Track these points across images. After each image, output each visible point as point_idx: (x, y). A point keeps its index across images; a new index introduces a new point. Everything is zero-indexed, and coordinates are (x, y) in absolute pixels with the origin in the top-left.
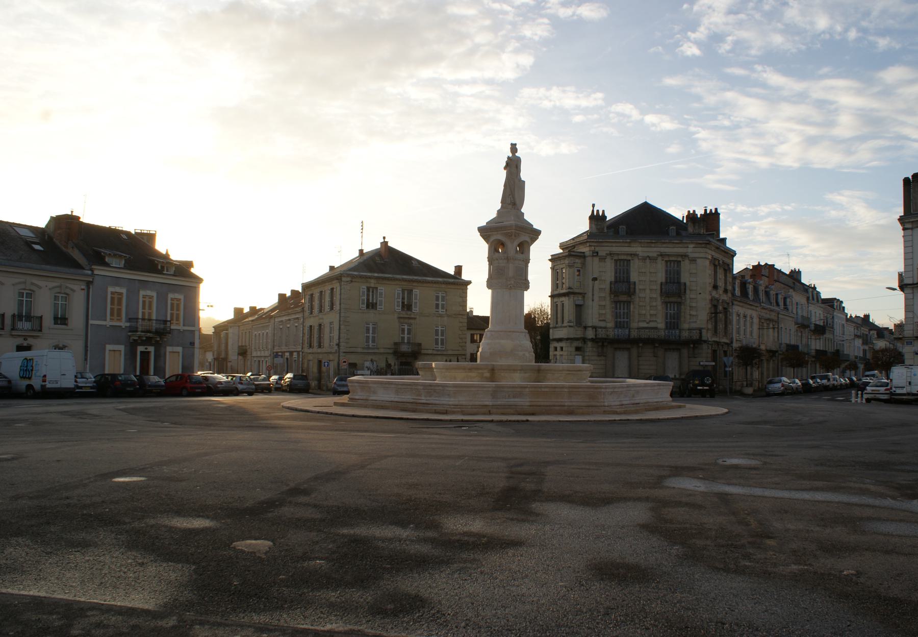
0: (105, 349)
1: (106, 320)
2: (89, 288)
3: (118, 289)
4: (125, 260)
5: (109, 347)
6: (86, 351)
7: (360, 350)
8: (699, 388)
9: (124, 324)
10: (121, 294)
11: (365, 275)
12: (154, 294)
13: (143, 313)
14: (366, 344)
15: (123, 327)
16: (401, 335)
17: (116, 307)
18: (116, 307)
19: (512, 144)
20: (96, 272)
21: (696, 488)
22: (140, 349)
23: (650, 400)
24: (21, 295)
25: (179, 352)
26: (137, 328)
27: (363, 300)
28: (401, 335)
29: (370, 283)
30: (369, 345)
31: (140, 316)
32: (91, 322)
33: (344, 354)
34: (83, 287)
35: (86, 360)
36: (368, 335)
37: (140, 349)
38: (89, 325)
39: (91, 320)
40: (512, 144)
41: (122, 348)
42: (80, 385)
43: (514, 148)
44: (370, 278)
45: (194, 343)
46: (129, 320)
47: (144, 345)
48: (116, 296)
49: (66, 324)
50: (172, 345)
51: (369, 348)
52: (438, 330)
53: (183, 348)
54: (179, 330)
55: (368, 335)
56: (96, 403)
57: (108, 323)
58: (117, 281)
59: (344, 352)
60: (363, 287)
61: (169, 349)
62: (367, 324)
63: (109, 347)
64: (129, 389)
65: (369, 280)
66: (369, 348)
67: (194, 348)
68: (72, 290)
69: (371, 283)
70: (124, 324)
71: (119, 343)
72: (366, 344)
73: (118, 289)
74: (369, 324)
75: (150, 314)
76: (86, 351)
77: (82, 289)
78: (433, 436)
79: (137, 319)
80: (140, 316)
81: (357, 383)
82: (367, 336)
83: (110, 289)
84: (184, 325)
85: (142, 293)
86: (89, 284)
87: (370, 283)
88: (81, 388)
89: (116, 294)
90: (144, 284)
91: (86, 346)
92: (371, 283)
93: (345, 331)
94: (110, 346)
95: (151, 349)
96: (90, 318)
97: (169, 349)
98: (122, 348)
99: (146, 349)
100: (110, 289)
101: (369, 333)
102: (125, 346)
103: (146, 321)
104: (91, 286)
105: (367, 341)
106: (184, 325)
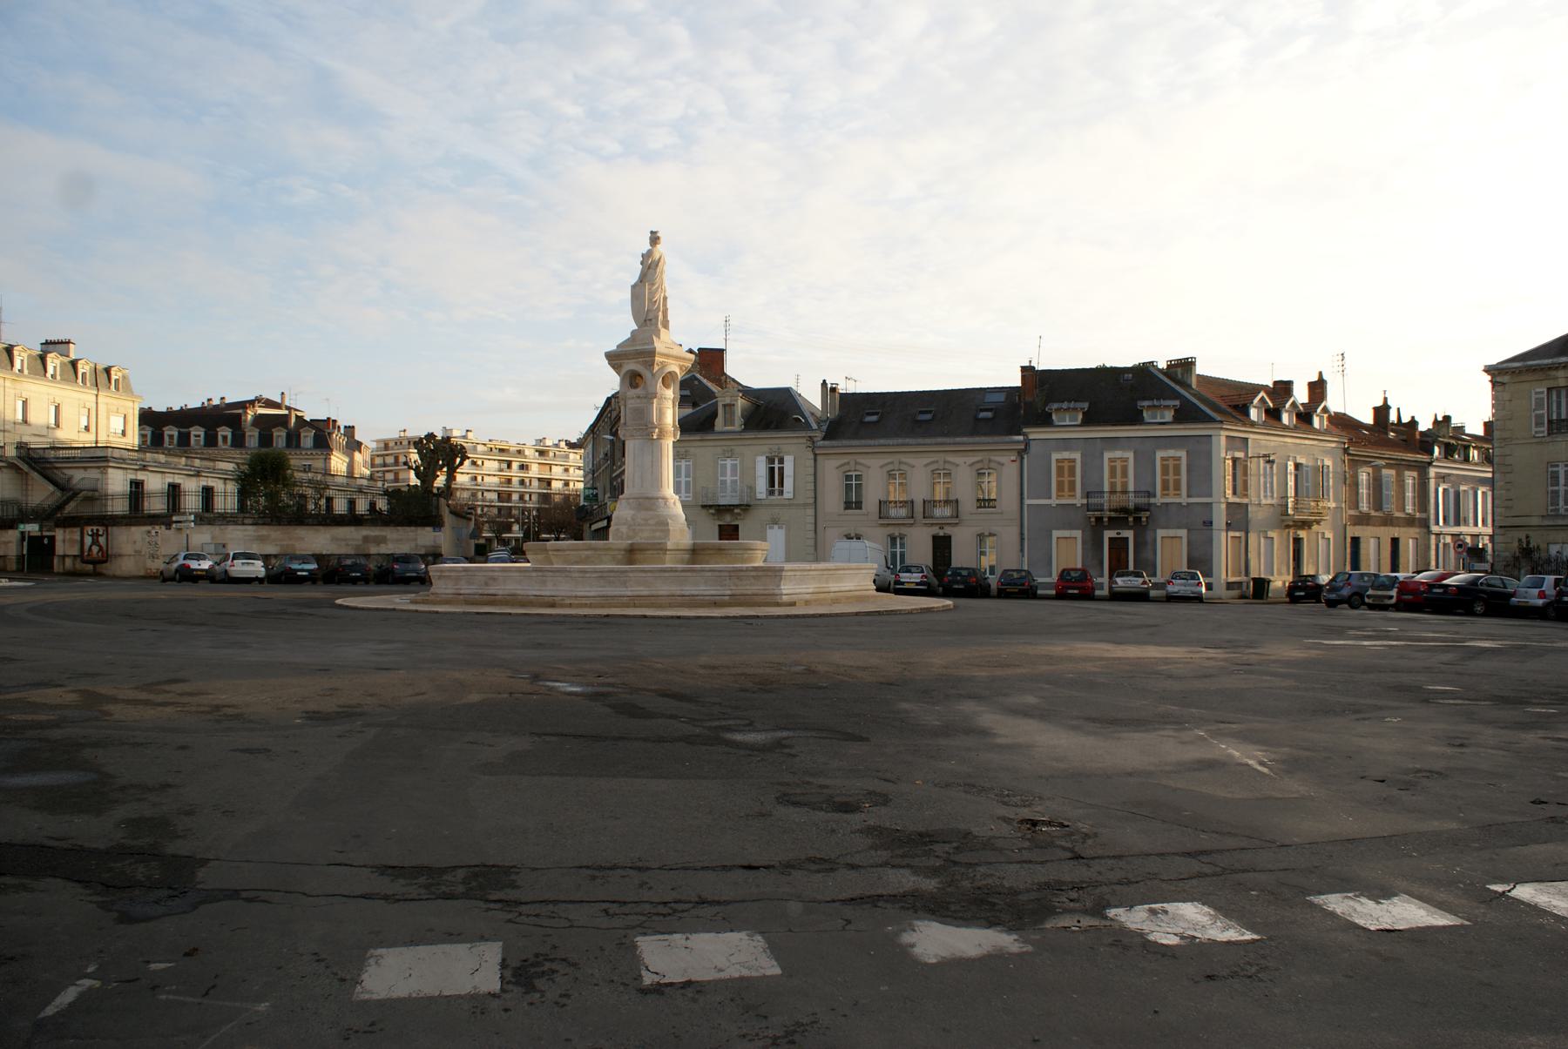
0: (1051, 535)
1: (1050, 498)
2: (1022, 458)
3: (1066, 455)
4: (1083, 413)
5: (1056, 534)
6: (1022, 539)
7: (1535, 521)
8: (1302, 594)
9: (1079, 500)
10: (1074, 461)
11: (1539, 365)
12: (1130, 455)
13: (1112, 485)
14: (1550, 508)
15: (1185, 504)
16: (1550, 488)
17: (1171, 477)
18: (1066, 479)
19: (652, 232)
20: (1031, 437)
21: (420, 697)
22: (1109, 534)
23: (519, 592)
24: (848, 478)
25: (1076, 538)
26: (1102, 505)
27: (1539, 417)
28: (1550, 488)
29: (1556, 378)
30: (1558, 510)
31: (1106, 488)
32: (1027, 502)
33: (1502, 531)
34: (1013, 458)
35: (1022, 550)
36: (1556, 488)
37: (1109, 534)
38: (1026, 506)
39: (1028, 498)
40: (652, 232)
41: (1078, 534)
42: (902, 580)
43: (655, 239)
44: (1550, 368)
45: (1211, 523)
46: (1088, 495)
47: (1115, 529)
48: (1066, 465)
49: (861, 508)
50: (1167, 527)
51: (1558, 516)
52: (1168, 480)
53: (1189, 530)
54: (1180, 503)
55: (1556, 488)
56: (1533, 626)
57: (1054, 501)
58: (1066, 444)
59: (1501, 527)
60: (1538, 390)
61: (1161, 533)
62: (1552, 466)
63: (1056, 534)
64: (956, 587)
65: (1553, 373)
66: (1558, 516)
67: (1212, 529)
68: (999, 463)
69: (1557, 378)
70: (1079, 500)
71: (1071, 527)
72: (1550, 508)
73: (1066, 455)
74: (1557, 466)
75: (1125, 484)
76: (1022, 539)
77: (1013, 461)
78: (1265, 678)
79: (1103, 492)
80: (1106, 488)
81: (516, 571)
82: (1552, 492)
83: (1055, 456)
84: (1189, 496)
85: (1107, 455)
86: (1021, 454)
87: (1556, 378)
88: (903, 583)
89: (1066, 462)
90: (1113, 443)
91: (1022, 534)
92: (1557, 378)
93: (1502, 483)
94: (1057, 531)
95: (1129, 534)
96: (1026, 497)
97: (1161, 533)
98: (1078, 534)
99: (1118, 534)
100: (1055, 456)
101: (1558, 485)
102: (1083, 532)
103: (1118, 495)
104: (1025, 456)
105: (1555, 502)
106: (1189, 496)
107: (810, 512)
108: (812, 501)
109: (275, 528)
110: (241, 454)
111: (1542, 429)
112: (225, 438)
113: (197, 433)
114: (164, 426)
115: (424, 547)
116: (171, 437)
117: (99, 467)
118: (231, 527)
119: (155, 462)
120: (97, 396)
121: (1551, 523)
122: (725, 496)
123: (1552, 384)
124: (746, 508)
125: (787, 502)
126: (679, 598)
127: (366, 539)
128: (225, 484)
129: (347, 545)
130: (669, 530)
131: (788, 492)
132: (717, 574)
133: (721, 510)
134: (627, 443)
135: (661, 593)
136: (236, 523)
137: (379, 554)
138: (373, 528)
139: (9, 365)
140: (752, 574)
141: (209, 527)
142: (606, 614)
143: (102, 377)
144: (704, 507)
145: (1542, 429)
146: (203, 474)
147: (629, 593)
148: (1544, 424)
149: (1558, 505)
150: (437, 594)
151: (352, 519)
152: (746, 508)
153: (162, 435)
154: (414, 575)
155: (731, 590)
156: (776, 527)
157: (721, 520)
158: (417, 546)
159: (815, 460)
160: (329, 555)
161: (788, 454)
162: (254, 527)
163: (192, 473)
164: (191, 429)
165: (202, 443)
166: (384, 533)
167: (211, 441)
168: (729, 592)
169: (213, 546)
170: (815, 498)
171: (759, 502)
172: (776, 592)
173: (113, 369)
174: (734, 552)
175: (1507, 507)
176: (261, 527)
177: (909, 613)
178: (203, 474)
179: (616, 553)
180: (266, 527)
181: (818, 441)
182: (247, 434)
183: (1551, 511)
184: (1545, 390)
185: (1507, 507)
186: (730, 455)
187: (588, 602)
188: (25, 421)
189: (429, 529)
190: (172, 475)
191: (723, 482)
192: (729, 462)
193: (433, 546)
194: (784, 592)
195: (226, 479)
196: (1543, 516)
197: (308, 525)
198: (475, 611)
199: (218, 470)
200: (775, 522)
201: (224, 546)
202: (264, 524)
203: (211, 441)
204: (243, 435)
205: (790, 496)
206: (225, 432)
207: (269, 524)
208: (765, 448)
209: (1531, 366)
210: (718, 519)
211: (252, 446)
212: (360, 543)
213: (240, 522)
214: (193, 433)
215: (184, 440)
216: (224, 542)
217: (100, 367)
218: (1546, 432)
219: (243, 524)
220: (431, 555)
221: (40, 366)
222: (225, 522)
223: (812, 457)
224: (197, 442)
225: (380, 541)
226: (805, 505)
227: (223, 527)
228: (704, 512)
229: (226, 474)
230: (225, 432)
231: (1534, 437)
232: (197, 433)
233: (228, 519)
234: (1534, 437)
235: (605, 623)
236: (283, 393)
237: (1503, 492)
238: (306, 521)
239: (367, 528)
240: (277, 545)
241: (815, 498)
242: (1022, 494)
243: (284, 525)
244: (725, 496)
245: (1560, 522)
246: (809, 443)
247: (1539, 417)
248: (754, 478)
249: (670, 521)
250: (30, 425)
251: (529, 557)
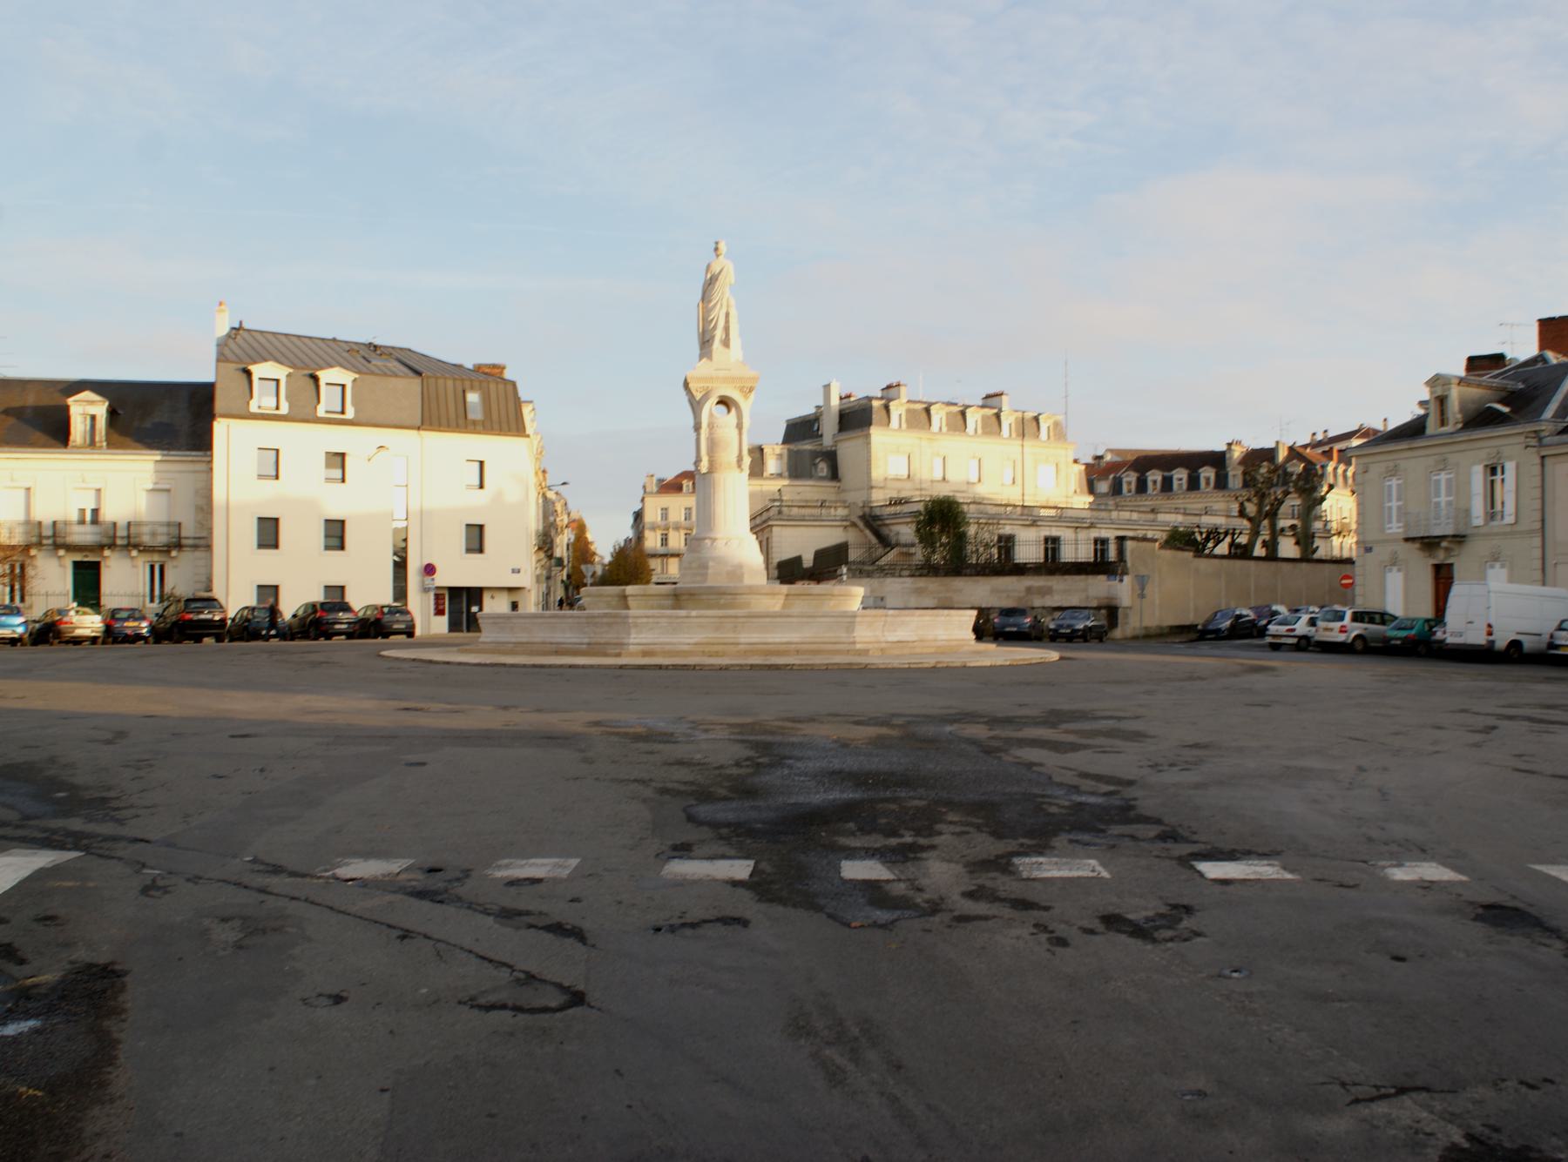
107: (1537, 541)
108: (1538, 525)
109: (934, 579)
110: (1223, 496)
112: (1208, 479)
113: (1180, 476)
114: (1147, 471)
115: (1096, 598)
116: (1155, 482)
118: (889, 580)
119: (981, 513)
120: (1023, 446)
122: (1439, 524)
124: (1459, 539)
125: (1508, 529)
126: (548, 645)
127: (1029, 590)
128: (1076, 533)
129: (1008, 597)
130: (706, 574)
131: (1478, 517)
132: (577, 620)
133: (1429, 544)
135: (536, 640)
136: (893, 575)
137: (1044, 608)
138: (1036, 578)
139: (928, 424)
140: (605, 620)
141: (868, 580)
142: (532, 663)
143: (1031, 426)
144: (1407, 540)
146: (1099, 526)
147: (513, 640)
151: (1052, 564)
152: (1459, 539)
153: (1198, 478)
154: (1015, 629)
155: (590, 638)
156: (1498, 565)
157: (1434, 558)
158: (1088, 597)
159: (1543, 465)
160: (989, 609)
161: (1510, 459)
162: (913, 579)
163: (1028, 523)
164: (1174, 472)
165: (1185, 486)
166: (1049, 584)
167: (1193, 484)
168: (586, 640)
169: (872, 599)
170: (1543, 521)
171: (1476, 531)
172: (626, 641)
173: (1041, 417)
174: (704, 597)
176: (918, 579)
177: (721, 669)
178: (1099, 526)
179: (609, 599)
180: (924, 579)
181: (1545, 437)
182: (1231, 474)
186: (1442, 467)
187: (707, 650)
188: (944, 479)
189: (1102, 578)
190: (1048, 528)
191: (1438, 504)
192: (1443, 477)
193: (1107, 598)
194: (632, 641)
195: (1077, 528)
197: (966, 575)
198: (413, 657)
199: (1066, 517)
200: (1495, 558)
201: (882, 599)
202: (921, 576)
203: (1193, 484)
204: (1226, 476)
205: (1510, 519)
206: (1207, 473)
207: (925, 576)
208: (1483, 454)
210: (1430, 556)
211: (1237, 487)
212: (1022, 594)
213: (897, 574)
214: (1175, 477)
215: (1167, 485)
216: (882, 595)
217: (1030, 415)
219: (900, 576)
220: (1105, 608)
221: (961, 422)
222: (882, 575)
223: (1538, 461)
224: (1180, 485)
225: (1047, 591)
226: (1530, 532)
227: (882, 580)
228: (1409, 545)
229: (1077, 522)
230: (1207, 473)
232: (1180, 475)
233: (886, 572)
236: (1385, 420)
238: (964, 571)
239: (1029, 577)
240: (934, 598)
241: (1543, 521)
243: (971, 575)
244: (1439, 524)
246: (1533, 442)
248: (1469, 498)
249: (711, 564)
250: (948, 482)
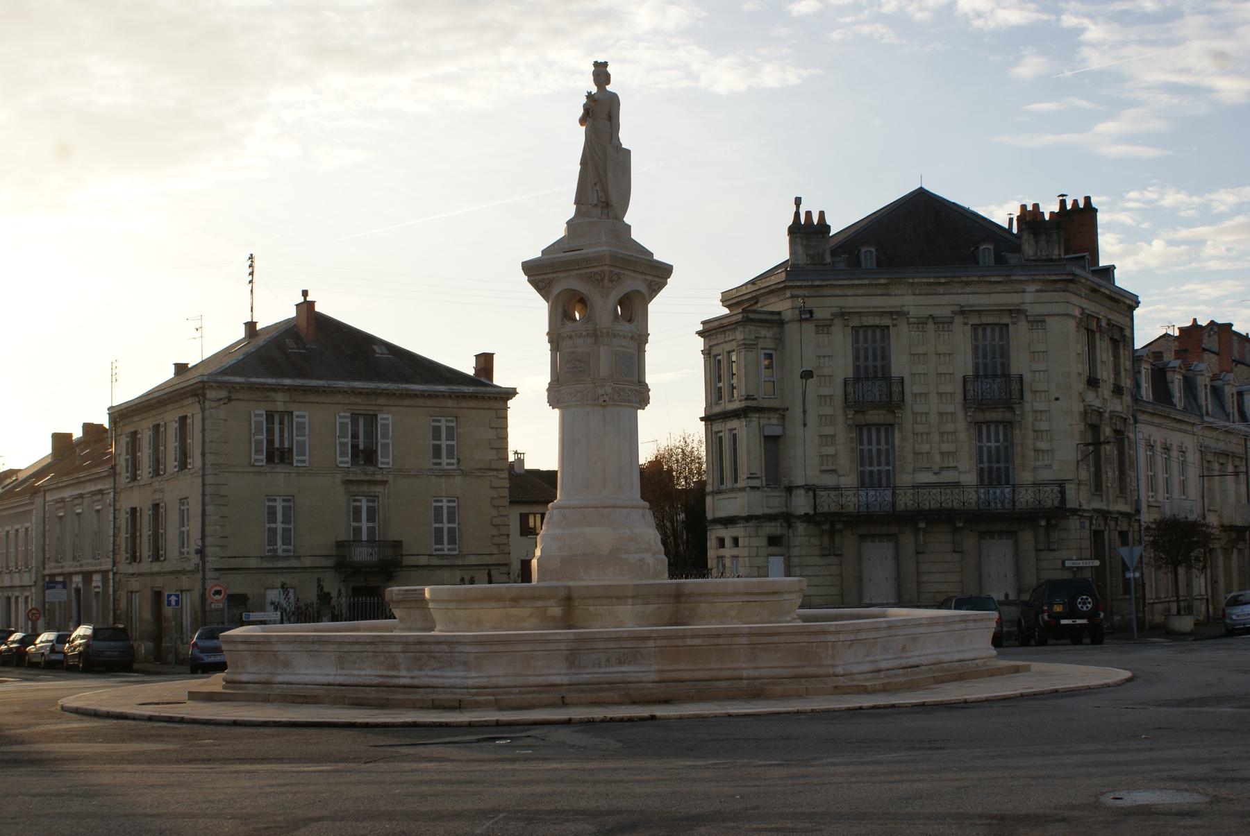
7: (253, 563)
14: (268, 548)
16: (267, 526)
28: (267, 526)
30: (276, 550)
36: (273, 525)
44: (274, 389)
51: (275, 557)
55: (273, 525)
60: (257, 412)
65: (272, 394)
66: (275, 557)
72: (268, 548)
74: (275, 500)
82: (269, 529)
101: (275, 522)
105: (272, 541)
111: (261, 457)
117: (1090, 478)
121: (270, 565)
123: (271, 407)
134: (1246, 502)
145: (261, 457)
148: (263, 451)
149: (276, 545)
150: (851, 674)
175: (222, 546)
183: (269, 551)
184: (264, 413)
185: (222, 546)
196: (262, 558)
209: (255, 384)
218: (265, 460)
231: (253, 466)
234: (253, 466)
235: (954, 708)
236: (251, 257)
237: (218, 528)
242: (165, 513)
245: (280, 564)
247: (259, 443)
251: (396, 612)
